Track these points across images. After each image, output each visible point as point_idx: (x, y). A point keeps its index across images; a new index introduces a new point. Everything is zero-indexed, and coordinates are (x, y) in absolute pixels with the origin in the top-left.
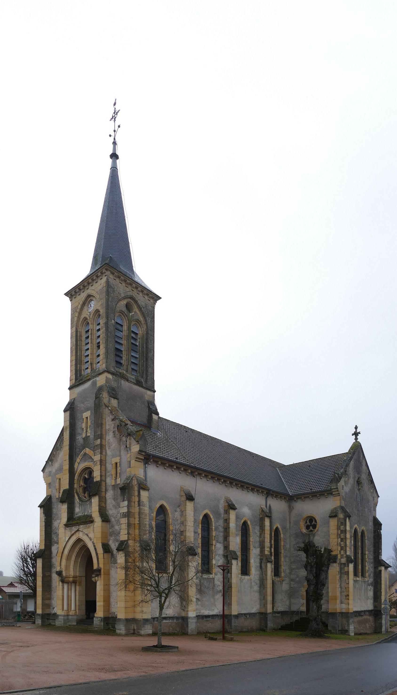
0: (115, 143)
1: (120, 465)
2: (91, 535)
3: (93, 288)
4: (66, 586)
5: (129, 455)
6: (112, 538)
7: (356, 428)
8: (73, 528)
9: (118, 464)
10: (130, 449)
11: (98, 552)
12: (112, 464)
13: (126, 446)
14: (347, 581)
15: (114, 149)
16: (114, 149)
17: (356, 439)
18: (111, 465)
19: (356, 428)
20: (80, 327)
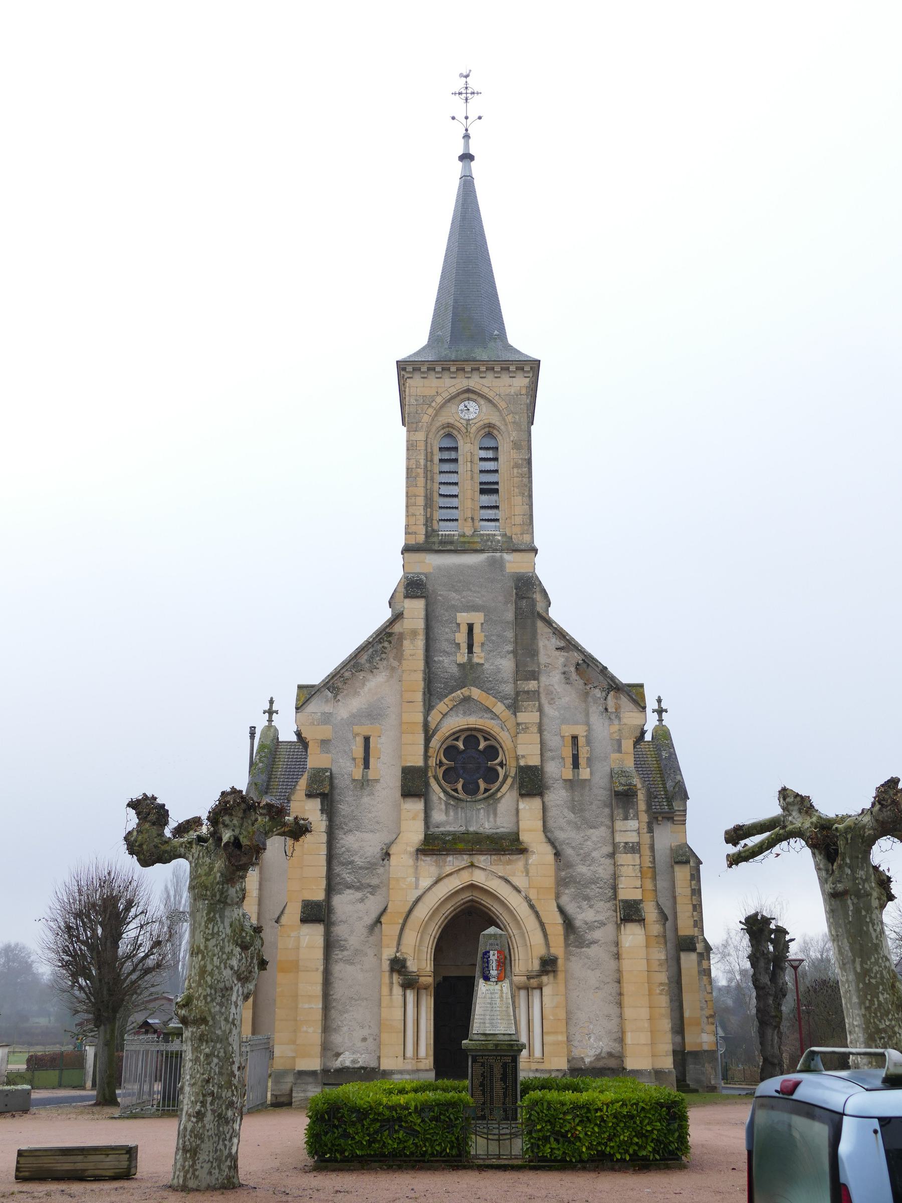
0: (467, 137)
1: (589, 742)
2: (519, 881)
3: (497, 382)
4: (411, 996)
5: (615, 728)
6: (567, 891)
7: (271, 702)
8: (450, 858)
9: (582, 741)
10: (619, 718)
11: (544, 920)
12: (563, 737)
13: (606, 709)
14: (708, 987)
15: (467, 145)
16: (467, 145)
17: (270, 720)
18: (558, 738)
19: (271, 702)
20: (431, 435)
